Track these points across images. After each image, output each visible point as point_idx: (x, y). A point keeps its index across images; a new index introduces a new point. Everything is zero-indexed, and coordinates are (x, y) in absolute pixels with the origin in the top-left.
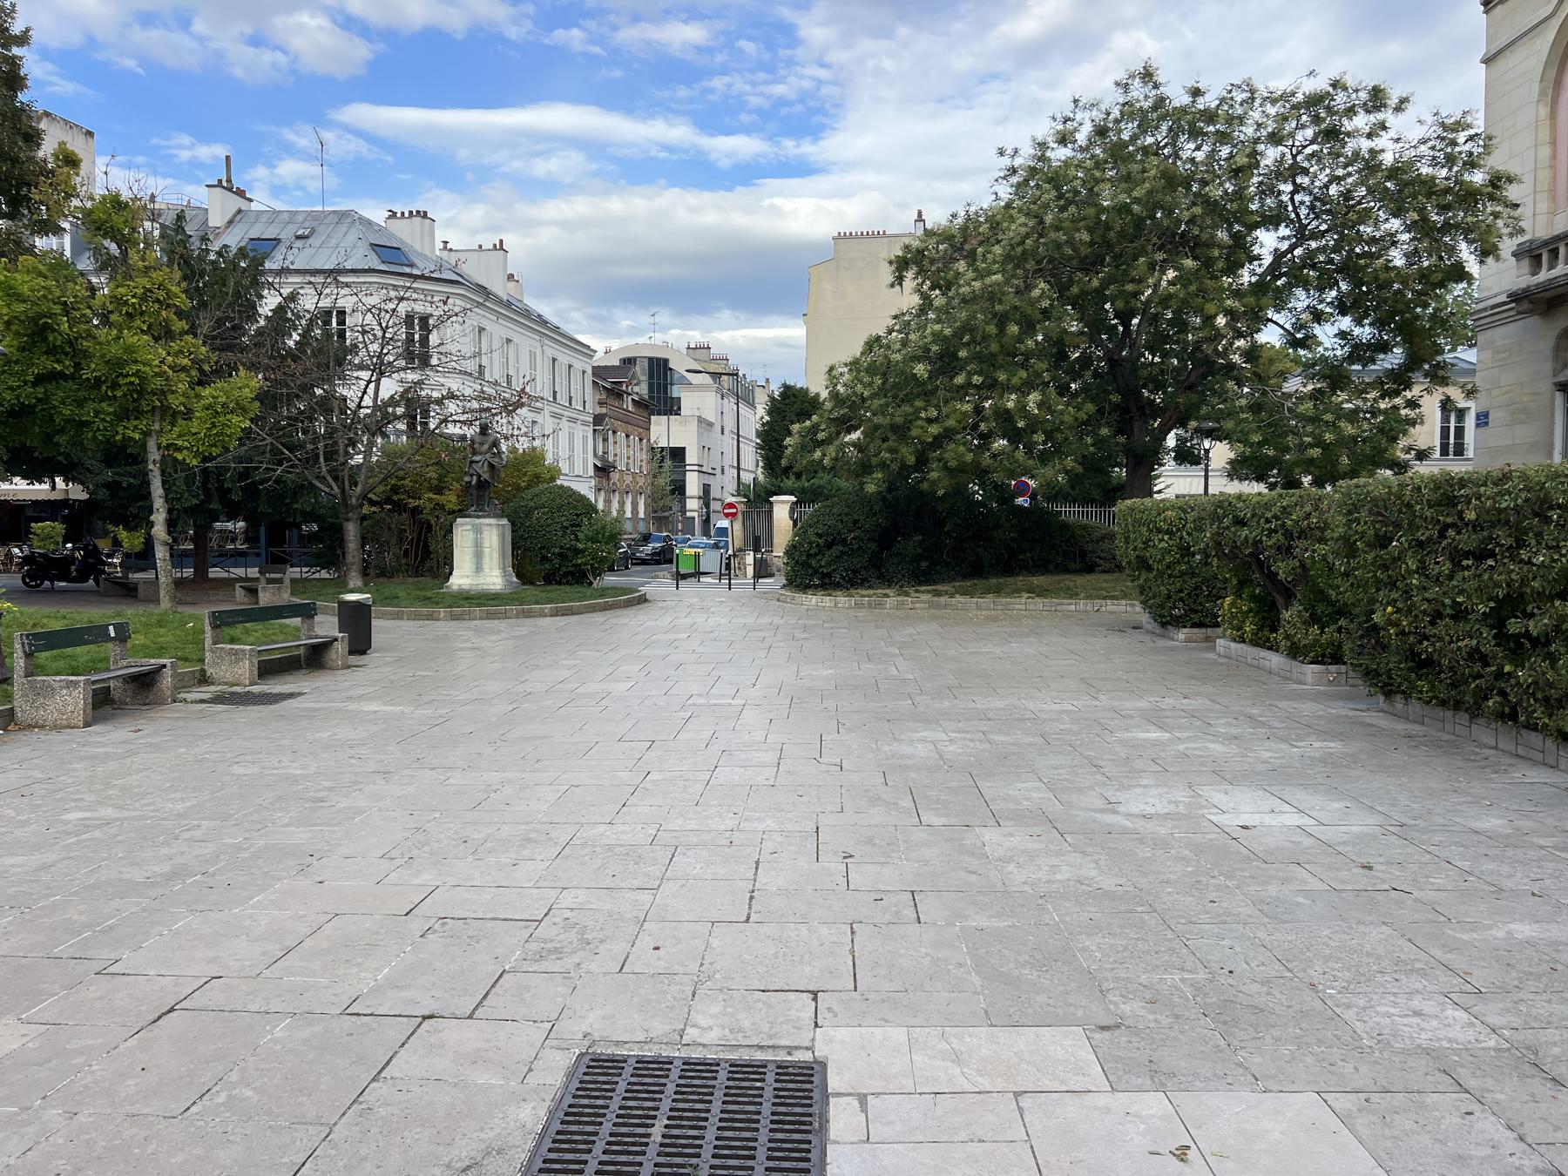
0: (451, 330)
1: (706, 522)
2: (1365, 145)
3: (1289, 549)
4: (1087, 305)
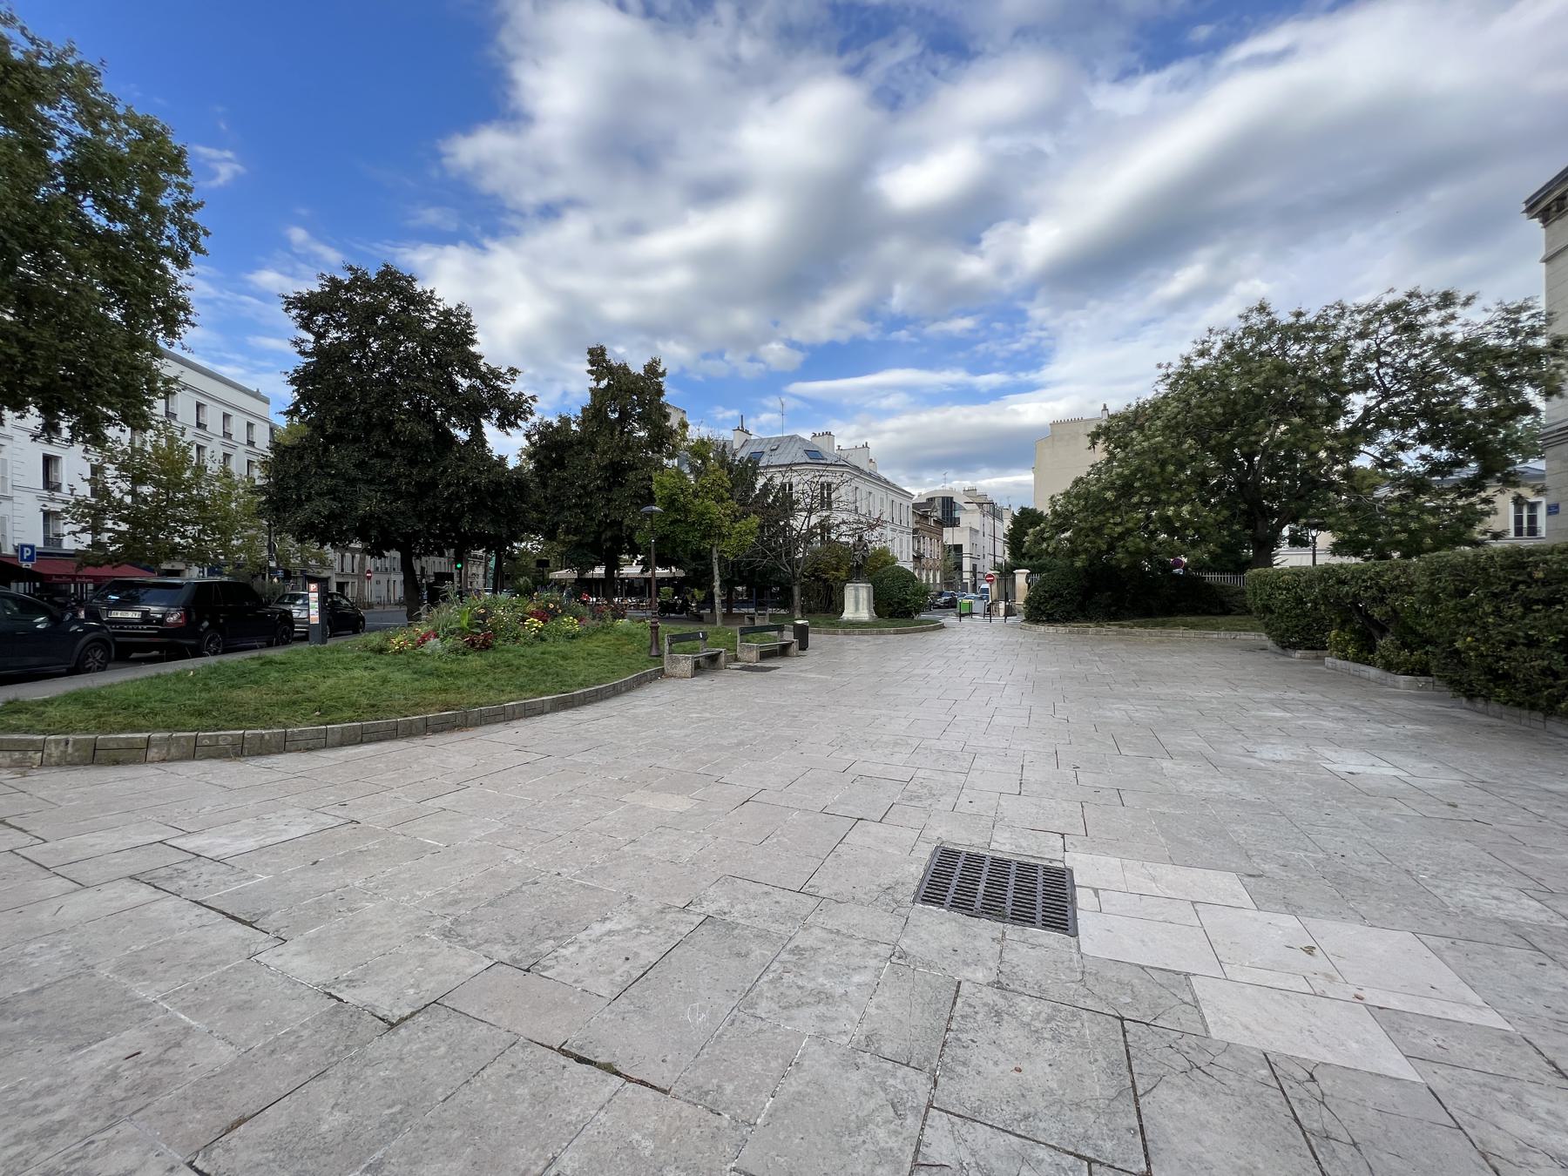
0: (842, 490)
1: (975, 585)
2: (1437, 331)
3: (1382, 600)
4: (1223, 453)
